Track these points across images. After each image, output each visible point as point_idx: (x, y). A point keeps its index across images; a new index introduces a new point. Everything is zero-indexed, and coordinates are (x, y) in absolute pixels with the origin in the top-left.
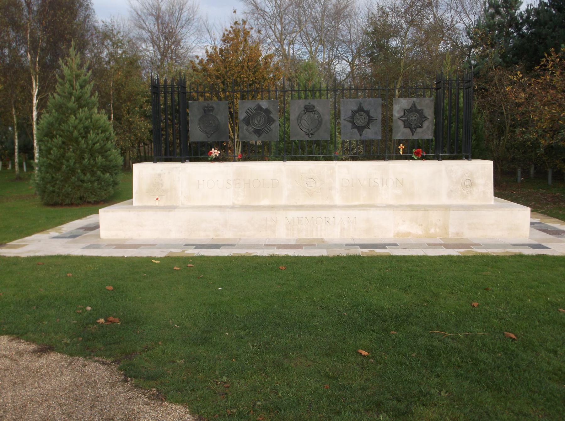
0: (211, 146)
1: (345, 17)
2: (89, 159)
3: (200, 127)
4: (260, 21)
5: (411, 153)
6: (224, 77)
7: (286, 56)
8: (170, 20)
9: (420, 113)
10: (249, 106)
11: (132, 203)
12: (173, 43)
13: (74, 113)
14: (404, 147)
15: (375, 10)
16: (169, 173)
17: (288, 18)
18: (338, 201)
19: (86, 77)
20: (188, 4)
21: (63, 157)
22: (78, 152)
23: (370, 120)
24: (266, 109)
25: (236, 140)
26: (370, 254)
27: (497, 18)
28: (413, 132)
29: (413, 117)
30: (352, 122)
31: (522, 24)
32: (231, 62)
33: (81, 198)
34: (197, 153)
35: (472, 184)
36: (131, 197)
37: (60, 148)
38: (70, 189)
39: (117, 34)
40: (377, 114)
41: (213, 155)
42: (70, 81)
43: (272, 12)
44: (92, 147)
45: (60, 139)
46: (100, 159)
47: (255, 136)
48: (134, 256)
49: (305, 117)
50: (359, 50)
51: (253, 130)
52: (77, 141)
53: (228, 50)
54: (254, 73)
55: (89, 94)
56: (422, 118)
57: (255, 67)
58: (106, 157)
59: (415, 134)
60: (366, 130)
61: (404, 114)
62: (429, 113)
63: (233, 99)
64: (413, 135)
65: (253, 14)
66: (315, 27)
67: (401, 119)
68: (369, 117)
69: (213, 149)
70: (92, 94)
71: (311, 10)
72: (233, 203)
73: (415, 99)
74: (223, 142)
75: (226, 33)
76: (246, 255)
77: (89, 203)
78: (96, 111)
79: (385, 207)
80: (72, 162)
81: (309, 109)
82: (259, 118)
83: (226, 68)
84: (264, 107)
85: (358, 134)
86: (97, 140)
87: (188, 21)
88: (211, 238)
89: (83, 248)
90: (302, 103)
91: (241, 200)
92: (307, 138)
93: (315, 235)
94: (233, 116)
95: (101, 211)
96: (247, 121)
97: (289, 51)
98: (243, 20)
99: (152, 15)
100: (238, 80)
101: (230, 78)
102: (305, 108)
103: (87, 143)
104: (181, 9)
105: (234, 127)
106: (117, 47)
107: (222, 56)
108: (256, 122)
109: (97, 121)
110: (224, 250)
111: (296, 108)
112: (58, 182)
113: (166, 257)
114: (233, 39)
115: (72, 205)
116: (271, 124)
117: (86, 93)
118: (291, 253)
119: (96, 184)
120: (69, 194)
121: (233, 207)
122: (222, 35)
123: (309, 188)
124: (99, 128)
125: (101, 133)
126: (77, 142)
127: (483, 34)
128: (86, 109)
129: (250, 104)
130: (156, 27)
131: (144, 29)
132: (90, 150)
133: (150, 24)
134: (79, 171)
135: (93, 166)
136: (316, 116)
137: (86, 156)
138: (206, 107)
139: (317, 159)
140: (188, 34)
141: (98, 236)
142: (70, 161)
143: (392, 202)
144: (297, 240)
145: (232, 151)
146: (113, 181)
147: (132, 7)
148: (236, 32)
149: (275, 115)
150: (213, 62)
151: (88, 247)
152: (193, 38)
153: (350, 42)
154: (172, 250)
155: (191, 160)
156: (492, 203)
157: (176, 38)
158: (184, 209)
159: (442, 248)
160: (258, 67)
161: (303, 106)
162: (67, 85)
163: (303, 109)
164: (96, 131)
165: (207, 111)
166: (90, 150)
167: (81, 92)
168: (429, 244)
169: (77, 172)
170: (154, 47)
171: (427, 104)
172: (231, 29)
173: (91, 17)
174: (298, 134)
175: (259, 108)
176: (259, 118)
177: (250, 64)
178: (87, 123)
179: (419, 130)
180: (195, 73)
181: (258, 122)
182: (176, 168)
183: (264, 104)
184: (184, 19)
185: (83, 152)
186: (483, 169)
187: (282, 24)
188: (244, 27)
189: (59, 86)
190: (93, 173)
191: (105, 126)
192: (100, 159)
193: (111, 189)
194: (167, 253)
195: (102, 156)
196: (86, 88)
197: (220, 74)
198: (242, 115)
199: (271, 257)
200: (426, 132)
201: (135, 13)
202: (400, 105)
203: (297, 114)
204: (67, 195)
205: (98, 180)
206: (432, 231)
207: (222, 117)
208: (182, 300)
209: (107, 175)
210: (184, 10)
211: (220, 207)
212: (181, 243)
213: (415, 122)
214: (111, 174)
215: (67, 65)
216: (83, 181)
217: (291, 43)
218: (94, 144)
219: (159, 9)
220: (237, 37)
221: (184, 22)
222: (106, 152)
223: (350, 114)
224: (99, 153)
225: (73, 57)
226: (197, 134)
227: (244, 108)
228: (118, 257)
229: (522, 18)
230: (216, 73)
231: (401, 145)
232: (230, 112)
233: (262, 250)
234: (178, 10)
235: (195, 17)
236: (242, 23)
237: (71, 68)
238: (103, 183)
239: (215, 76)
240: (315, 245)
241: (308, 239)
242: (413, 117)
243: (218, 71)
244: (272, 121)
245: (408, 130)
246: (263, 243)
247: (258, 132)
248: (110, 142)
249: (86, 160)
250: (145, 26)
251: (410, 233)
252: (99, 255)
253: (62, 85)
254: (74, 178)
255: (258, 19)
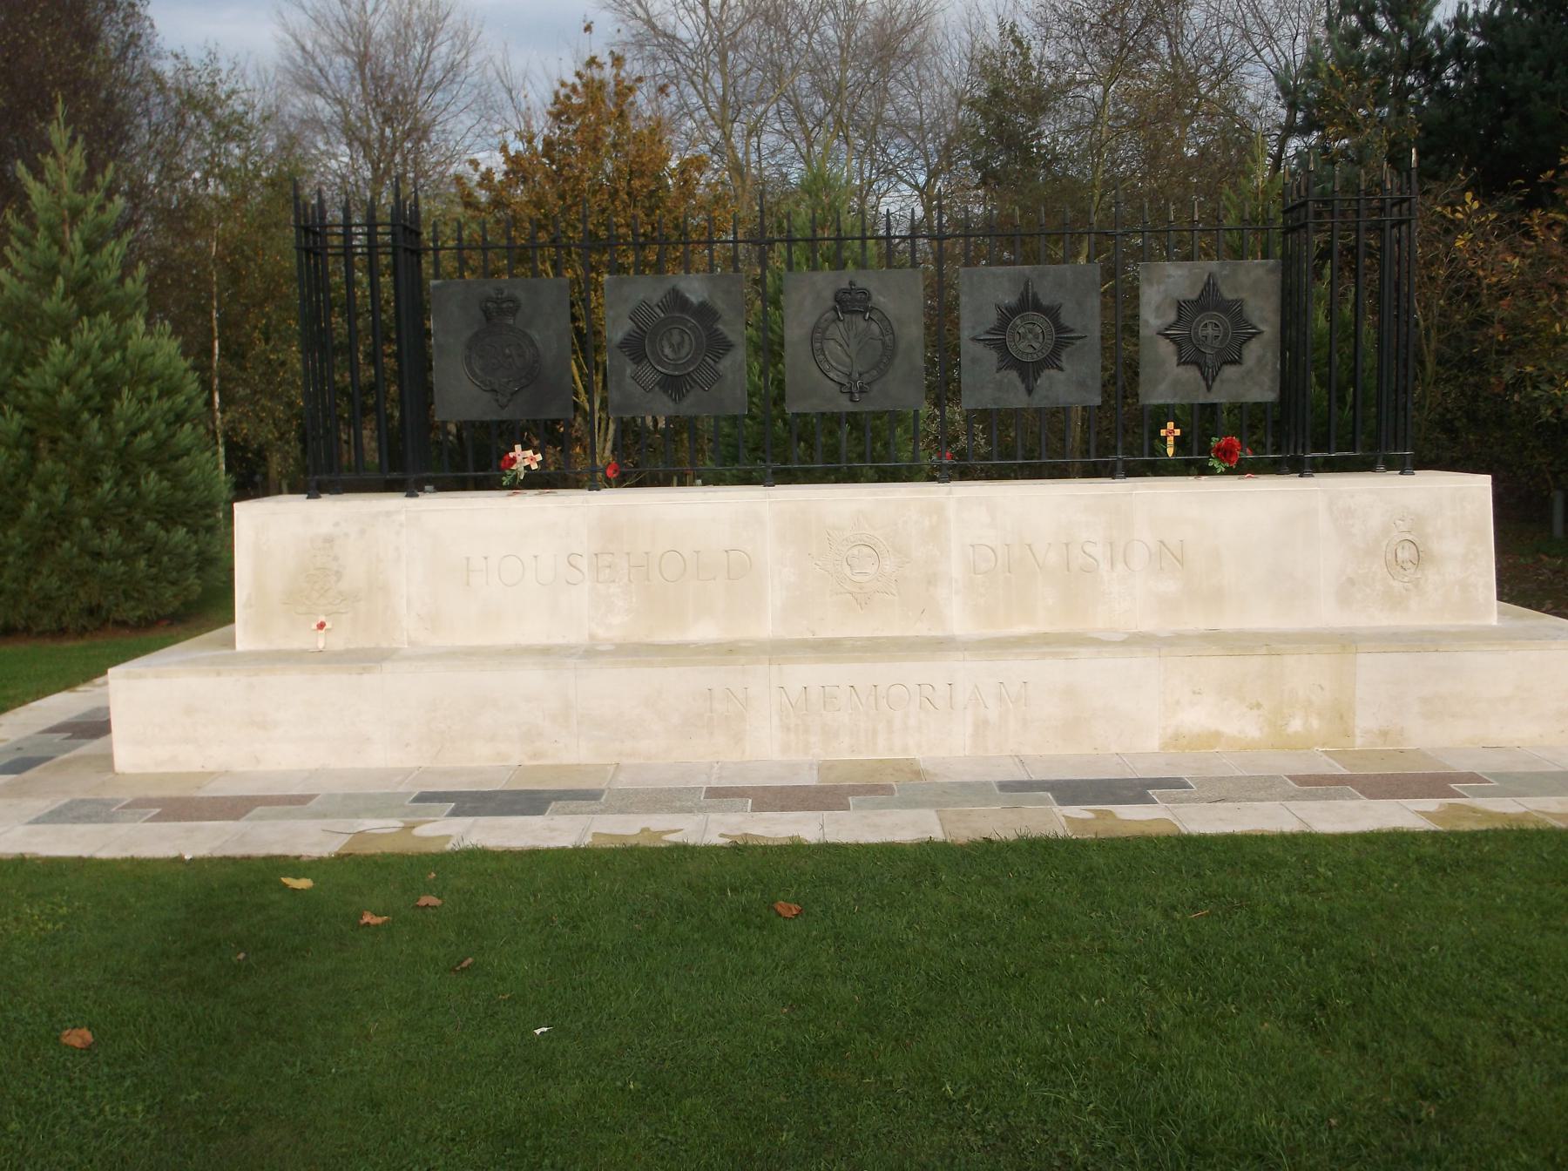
0: (513, 433)
1: (907, 58)
2: (117, 483)
3: (472, 371)
4: (663, 64)
5: (1205, 450)
6: (556, 226)
7: (738, 169)
8: (396, 66)
9: (1234, 312)
10: (641, 297)
11: (230, 642)
12: (407, 135)
13: (64, 329)
14: (1178, 432)
15: (992, 37)
16: (362, 532)
17: (738, 61)
18: (959, 623)
19: (105, 218)
20: (449, 21)
21: (30, 476)
22: (80, 461)
23: (1062, 339)
24: (703, 305)
25: (597, 416)
26: (1102, 830)
27: (1367, 43)
28: (1209, 380)
29: (1209, 329)
30: (1002, 348)
31: (1442, 62)
32: (577, 179)
33: (92, 611)
34: (469, 462)
35: (1421, 558)
36: (232, 621)
37: (17, 445)
38: (55, 582)
39: (229, 97)
40: (1086, 318)
41: (519, 467)
42: (50, 228)
43: (697, 39)
44: (127, 443)
45: (17, 416)
46: (152, 482)
47: (665, 398)
48: (218, 854)
49: (837, 331)
50: (946, 152)
51: (658, 377)
52: (73, 424)
53: (568, 143)
54: (650, 211)
55: (115, 273)
56: (1242, 331)
57: (652, 194)
58: (176, 478)
59: (1216, 385)
60: (1049, 373)
61: (1180, 318)
62: (1264, 313)
63: (588, 291)
64: (1209, 388)
65: (642, 46)
66: (819, 89)
67: (1167, 336)
68: (1060, 328)
69: (518, 447)
70: (127, 268)
71: (810, 37)
72: (592, 637)
73: (1214, 265)
74: (556, 422)
75: (563, 92)
76: (645, 842)
77: (123, 624)
78: (141, 325)
79: (1124, 643)
80: (58, 492)
81: (850, 303)
82: (676, 338)
83: (562, 197)
84: (694, 299)
85: (1022, 387)
86: (142, 420)
87: (452, 69)
88: (514, 762)
89: (37, 821)
90: (826, 282)
91: (617, 626)
92: (844, 405)
93: (886, 748)
94: (586, 342)
95: (110, 671)
96: (635, 348)
97: (746, 153)
98: (612, 53)
99: (345, 51)
100: (602, 233)
101: (575, 228)
102: (837, 299)
103: (112, 430)
104: (430, 35)
105: (590, 376)
106: (229, 137)
107: (552, 162)
108: (667, 351)
109: (143, 358)
110: (561, 821)
111: (807, 297)
112: (11, 559)
113: (340, 858)
114: (582, 111)
115: (61, 632)
116: (718, 357)
117: (107, 266)
118: (809, 828)
119: (142, 563)
120: (51, 599)
121: (591, 653)
122: (550, 99)
123: (857, 578)
124: (151, 380)
125: (160, 397)
126: (73, 424)
127: (1312, 99)
128: (105, 318)
129: (646, 290)
130: (358, 88)
131: (321, 91)
132: (121, 453)
133: (338, 78)
134: (86, 522)
135: (130, 506)
136: (875, 328)
137: (107, 470)
138: (489, 299)
139: (852, 477)
140: (452, 108)
141: (107, 760)
142: (54, 488)
143: (1148, 625)
144: (825, 767)
145: (584, 449)
146: (200, 553)
147: (287, 30)
148: (594, 89)
149: (735, 330)
150: (525, 180)
151: (55, 816)
152: (467, 120)
153: (920, 127)
154: (370, 824)
155: (443, 486)
156: (1493, 620)
157: (416, 120)
158: (413, 666)
159: (1353, 797)
160: (661, 193)
161: (828, 295)
162: (41, 241)
163: (831, 303)
164: (142, 389)
165: (496, 314)
166: (121, 453)
167: (87, 264)
168: (1303, 780)
169: (79, 526)
170: (350, 145)
171: (1254, 285)
172: (577, 81)
173: (142, 42)
174: (814, 389)
175: (677, 301)
176: (676, 338)
177: (636, 183)
178: (109, 364)
179: (1229, 371)
180: (470, 212)
181: (674, 350)
182: (388, 514)
183: (695, 288)
184: (438, 65)
185: (94, 459)
186: (1459, 505)
187: (724, 74)
188: (618, 75)
189: (19, 246)
190: (130, 529)
191: (171, 377)
192: (152, 482)
193: (192, 579)
194: (346, 839)
195: (161, 473)
196: (106, 251)
197: (546, 216)
198: (616, 328)
199: (739, 851)
200: (1253, 381)
201: (293, 44)
202: (1164, 287)
203: (810, 321)
204: (46, 603)
205: (149, 551)
206: (1296, 725)
207: (549, 334)
208: (375, 1106)
209: (181, 532)
210: (441, 37)
211: (545, 653)
212: (401, 789)
213: (1217, 344)
214: (193, 531)
215: (42, 181)
216: (97, 555)
217: (754, 131)
218: (134, 434)
219: (364, 35)
220: (591, 106)
221: (439, 75)
222: (177, 458)
223: (992, 318)
224: (151, 463)
225: (61, 151)
226: (459, 395)
227: (620, 307)
228: (155, 861)
229: (1440, 41)
230: (533, 213)
231: (1170, 425)
232: (578, 331)
233: (699, 818)
234: (421, 38)
235: (472, 60)
236: (609, 61)
237: (55, 189)
238: (165, 559)
239: (531, 221)
240: (887, 790)
241: (861, 763)
242: (1209, 329)
243: (538, 205)
244: (720, 346)
245: (1191, 373)
246: (702, 782)
247: (673, 385)
248: (188, 427)
249: (107, 486)
250: (324, 84)
251: (1217, 735)
252: (85, 853)
253: (27, 243)
254: (67, 544)
255: (655, 59)
